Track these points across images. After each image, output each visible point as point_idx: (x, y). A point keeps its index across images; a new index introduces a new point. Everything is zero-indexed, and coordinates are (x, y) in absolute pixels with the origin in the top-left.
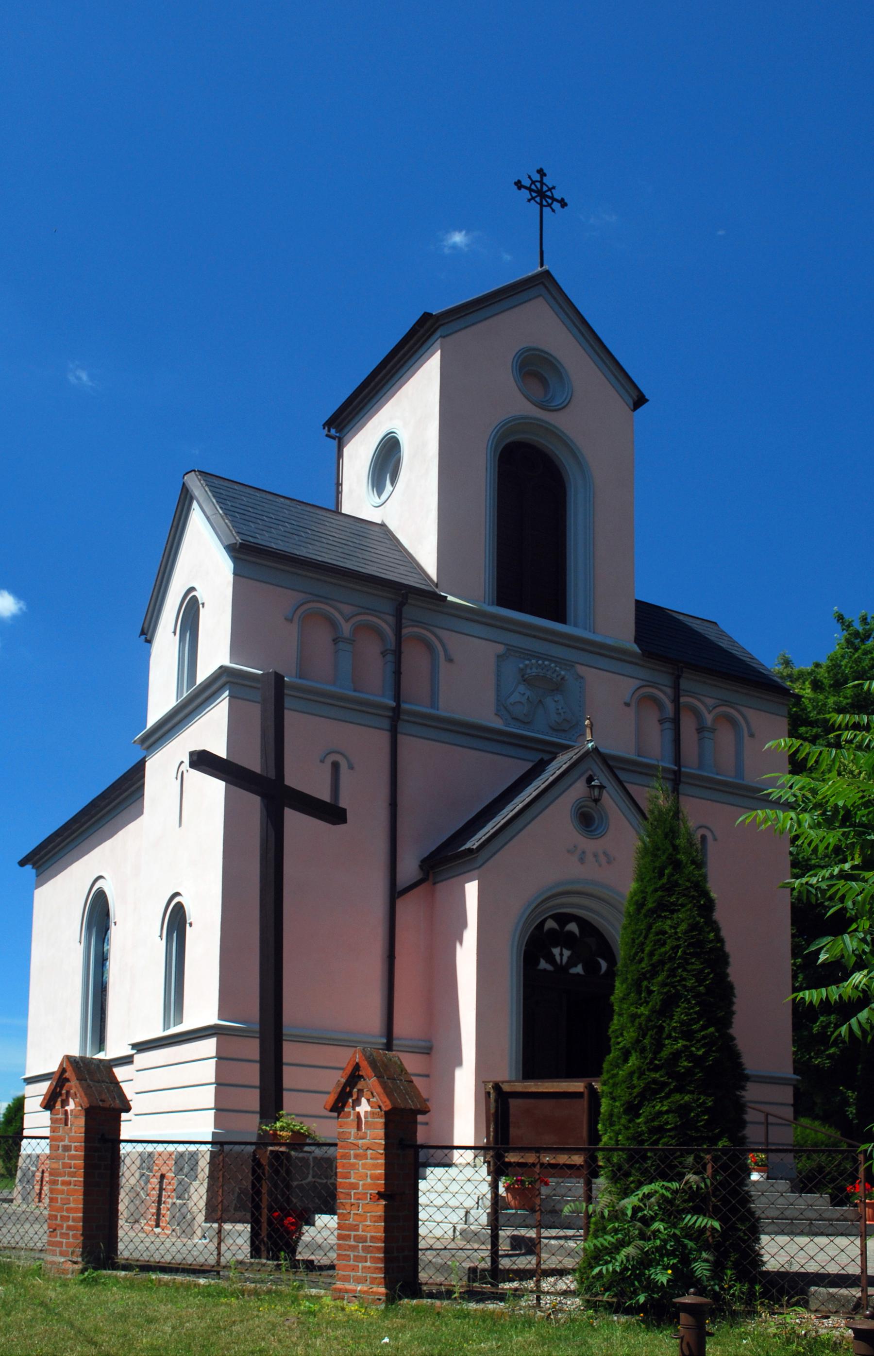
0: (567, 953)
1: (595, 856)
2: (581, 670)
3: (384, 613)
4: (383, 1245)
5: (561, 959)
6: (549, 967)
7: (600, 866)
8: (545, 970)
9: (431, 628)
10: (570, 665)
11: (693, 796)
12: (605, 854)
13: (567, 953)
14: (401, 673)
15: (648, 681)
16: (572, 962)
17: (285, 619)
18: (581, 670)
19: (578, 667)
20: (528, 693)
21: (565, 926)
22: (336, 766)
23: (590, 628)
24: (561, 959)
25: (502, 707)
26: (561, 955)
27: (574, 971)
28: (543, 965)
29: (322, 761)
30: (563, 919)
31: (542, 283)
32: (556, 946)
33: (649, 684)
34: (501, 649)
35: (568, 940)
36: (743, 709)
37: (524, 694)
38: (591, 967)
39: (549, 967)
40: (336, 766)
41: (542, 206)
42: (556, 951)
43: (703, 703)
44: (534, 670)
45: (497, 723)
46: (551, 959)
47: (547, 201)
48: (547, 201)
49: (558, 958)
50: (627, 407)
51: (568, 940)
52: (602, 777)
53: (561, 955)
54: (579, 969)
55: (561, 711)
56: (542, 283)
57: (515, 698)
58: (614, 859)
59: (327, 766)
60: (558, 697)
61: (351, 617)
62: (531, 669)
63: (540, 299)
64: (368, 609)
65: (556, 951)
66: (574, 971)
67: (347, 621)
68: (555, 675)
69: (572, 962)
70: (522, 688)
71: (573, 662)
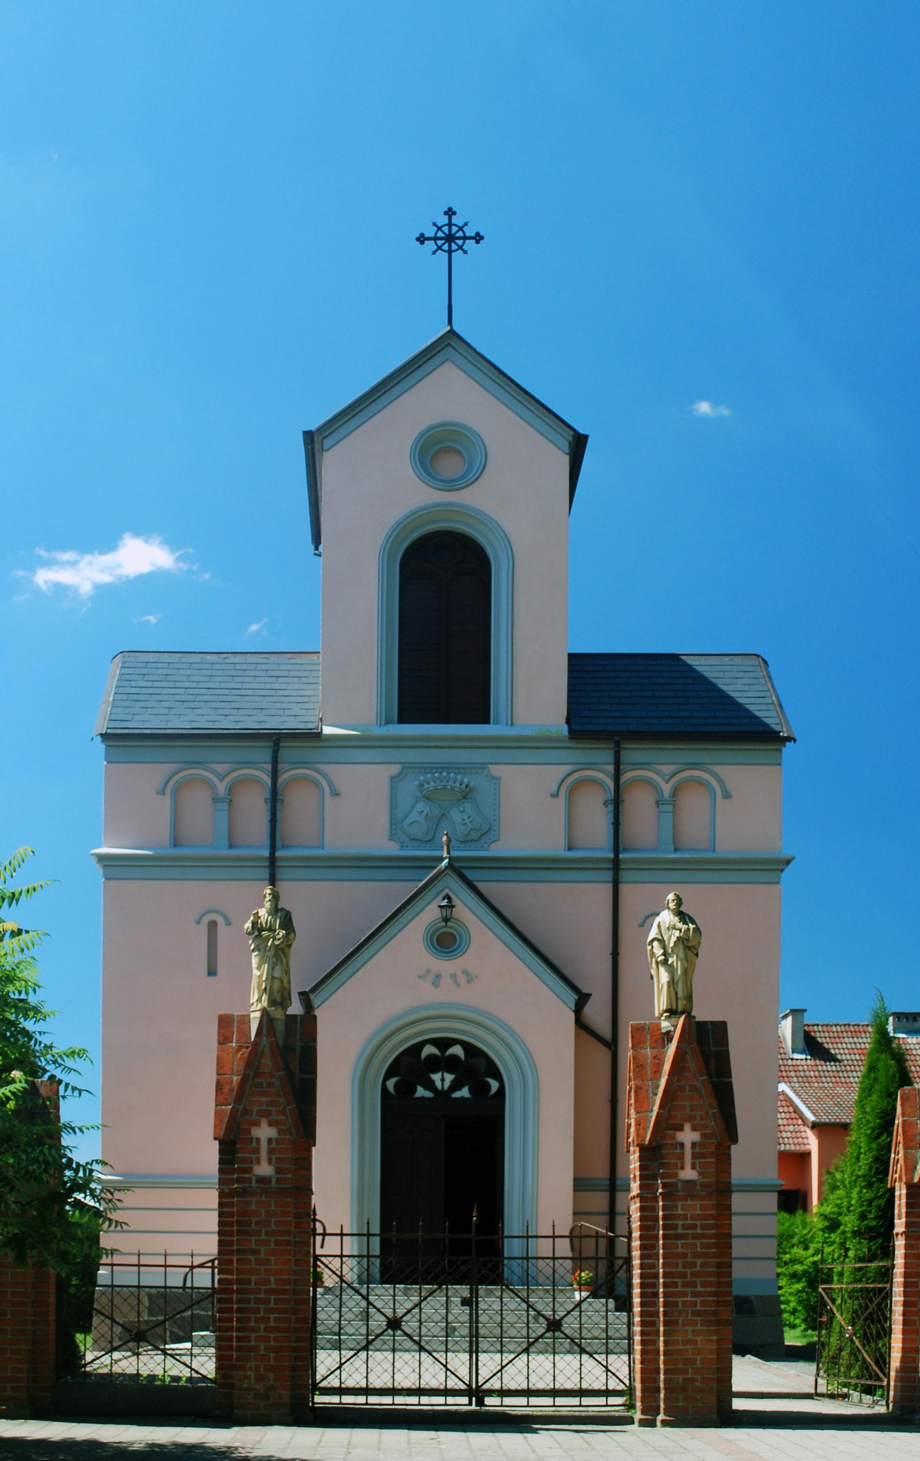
0: (449, 1078)
1: (453, 976)
2: (495, 770)
3: (264, 763)
4: (663, 1152)
5: (443, 1085)
6: (428, 1094)
7: (458, 985)
8: (423, 1098)
9: (310, 766)
10: (482, 767)
11: (643, 882)
12: (465, 972)
13: (449, 1078)
14: (619, 824)
15: (577, 764)
16: (455, 1086)
17: (158, 793)
18: (495, 770)
19: (491, 767)
20: (427, 810)
21: (445, 1052)
22: (213, 925)
23: (507, 722)
24: (443, 1085)
25: (395, 828)
26: (443, 1080)
27: (457, 1094)
28: (421, 1092)
29: (198, 922)
30: (443, 1043)
31: (449, 344)
32: (435, 1071)
33: (582, 766)
34: (395, 769)
35: (451, 1064)
36: (714, 768)
37: (422, 812)
38: (480, 1089)
39: (428, 1094)
40: (213, 925)
41: (450, 252)
42: (436, 1077)
43: (657, 772)
44: (432, 784)
45: (392, 849)
46: (430, 1086)
47: (457, 244)
48: (457, 244)
49: (438, 1084)
50: (560, 452)
51: (451, 1064)
52: (453, 884)
53: (443, 1080)
54: (465, 1092)
55: (467, 821)
56: (449, 344)
57: (413, 817)
58: (476, 977)
59: (204, 928)
60: (467, 806)
61: (227, 775)
62: (428, 784)
63: (448, 365)
64: (242, 763)
65: (436, 1077)
66: (457, 1094)
67: (221, 780)
68: (457, 785)
69: (455, 1086)
70: (420, 806)
71: (485, 763)
